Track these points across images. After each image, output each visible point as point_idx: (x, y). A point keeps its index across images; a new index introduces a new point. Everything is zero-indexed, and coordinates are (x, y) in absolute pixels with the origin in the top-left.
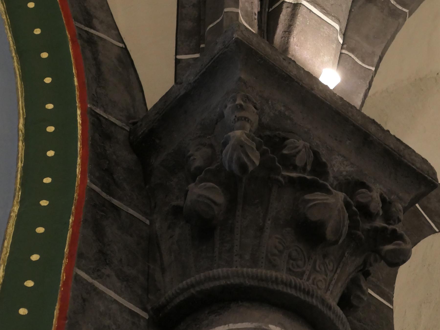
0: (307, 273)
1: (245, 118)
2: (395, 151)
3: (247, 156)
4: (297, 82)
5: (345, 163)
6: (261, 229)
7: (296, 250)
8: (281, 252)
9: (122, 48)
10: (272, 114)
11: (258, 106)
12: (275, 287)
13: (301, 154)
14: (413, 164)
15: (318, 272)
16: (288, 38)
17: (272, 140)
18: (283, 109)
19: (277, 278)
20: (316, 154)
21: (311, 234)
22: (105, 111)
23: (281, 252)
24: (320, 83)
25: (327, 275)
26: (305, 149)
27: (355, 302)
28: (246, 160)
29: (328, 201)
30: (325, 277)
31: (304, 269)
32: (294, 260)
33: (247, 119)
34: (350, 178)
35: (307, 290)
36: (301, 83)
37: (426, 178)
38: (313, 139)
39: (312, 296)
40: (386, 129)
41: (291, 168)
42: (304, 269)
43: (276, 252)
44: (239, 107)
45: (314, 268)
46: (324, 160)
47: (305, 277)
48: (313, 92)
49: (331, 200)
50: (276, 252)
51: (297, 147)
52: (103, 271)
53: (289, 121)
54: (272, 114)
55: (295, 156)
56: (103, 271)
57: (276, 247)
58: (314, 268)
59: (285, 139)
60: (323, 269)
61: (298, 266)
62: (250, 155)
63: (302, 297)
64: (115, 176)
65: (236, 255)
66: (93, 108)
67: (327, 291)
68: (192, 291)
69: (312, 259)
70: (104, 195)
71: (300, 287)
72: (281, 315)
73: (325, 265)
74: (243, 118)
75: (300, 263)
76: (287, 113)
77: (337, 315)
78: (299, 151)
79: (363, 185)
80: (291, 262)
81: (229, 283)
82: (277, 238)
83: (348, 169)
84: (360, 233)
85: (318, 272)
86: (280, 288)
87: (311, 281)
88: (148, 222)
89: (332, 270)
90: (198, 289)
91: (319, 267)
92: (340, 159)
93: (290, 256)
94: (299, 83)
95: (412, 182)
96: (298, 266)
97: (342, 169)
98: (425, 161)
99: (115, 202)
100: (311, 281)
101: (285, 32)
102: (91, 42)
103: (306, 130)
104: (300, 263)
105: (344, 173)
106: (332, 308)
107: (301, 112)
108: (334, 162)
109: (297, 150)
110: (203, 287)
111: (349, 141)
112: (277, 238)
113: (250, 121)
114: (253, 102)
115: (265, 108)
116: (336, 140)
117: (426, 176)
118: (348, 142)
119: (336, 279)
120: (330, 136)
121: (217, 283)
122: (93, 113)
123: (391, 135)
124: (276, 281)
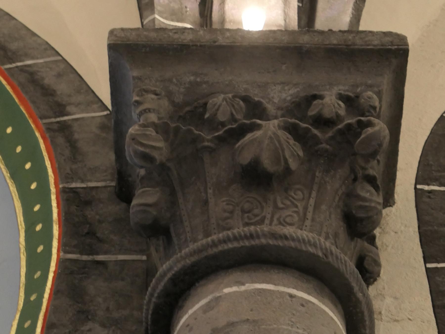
0: (269, 216)
1: (145, 111)
2: (339, 45)
3: (142, 145)
4: (192, 46)
5: (286, 88)
6: (206, 202)
7: (248, 201)
8: (232, 212)
9: (107, 115)
10: (182, 90)
11: (158, 90)
12: (215, 250)
13: (221, 109)
14: (368, 45)
15: (282, 209)
16: (224, 8)
17: (193, 111)
18: (192, 78)
19: (213, 241)
20: (246, 99)
21: (256, 178)
22: (83, 182)
23: (232, 212)
24: (244, 30)
25: (296, 206)
26: (226, 101)
27: (361, 214)
28: (141, 149)
29: (255, 136)
30: (296, 209)
31: (263, 214)
32: (249, 212)
33: (147, 111)
34: (297, 100)
35: (248, 235)
36: (199, 44)
37: (391, 49)
38: (239, 86)
39: (258, 237)
40: (326, 29)
41: (220, 127)
42: (263, 214)
43: (227, 215)
44: (136, 104)
45: (276, 207)
46: (256, 99)
47: (267, 221)
48: (217, 44)
49: (377, 128)
50: (227, 215)
51: (215, 105)
52: (82, 329)
53: (204, 86)
54: (182, 90)
55: (216, 115)
56: (82, 329)
57: (225, 211)
58: (276, 207)
59: (206, 104)
60: (288, 203)
61: (256, 216)
62: (145, 142)
63: (247, 243)
64: (99, 235)
65: (190, 242)
66: (66, 185)
67: (304, 221)
68: (154, 300)
69: (270, 200)
70: (85, 258)
71: (240, 236)
72: (239, 273)
73: (290, 198)
74: (143, 112)
75: (256, 211)
76: (198, 80)
77: (299, 241)
78: (220, 106)
79: (315, 97)
80: (246, 215)
81: (173, 272)
82: (224, 201)
83: (293, 91)
84: (324, 145)
85: (282, 209)
86: (220, 248)
87: (275, 222)
88: (144, 258)
89: (303, 199)
90: (156, 295)
91: (282, 203)
92: (279, 87)
93: (243, 211)
94: (196, 46)
95: (379, 62)
96: (256, 216)
97: (284, 95)
98: (389, 34)
99: (100, 258)
100: (275, 222)
101: (220, 4)
102: (64, 129)
103: (227, 83)
104: (256, 211)
105: (289, 98)
106: (288, 236)
107: (216, 70)
108: (272, 95)
109: (216, 107)
110: (158, 291)
111: (285, 65)
112: (224, 201)
113: (151, 110)
114: (152, 91)
115: (171, 89)
116: (269, 72)
117: (390, 47)
118: (284, 67)
119: (313, 205)
120: (259, 73)
121: (166, 279)
122: (67, 190)
123: (327, 32)
124: (214, 244)
